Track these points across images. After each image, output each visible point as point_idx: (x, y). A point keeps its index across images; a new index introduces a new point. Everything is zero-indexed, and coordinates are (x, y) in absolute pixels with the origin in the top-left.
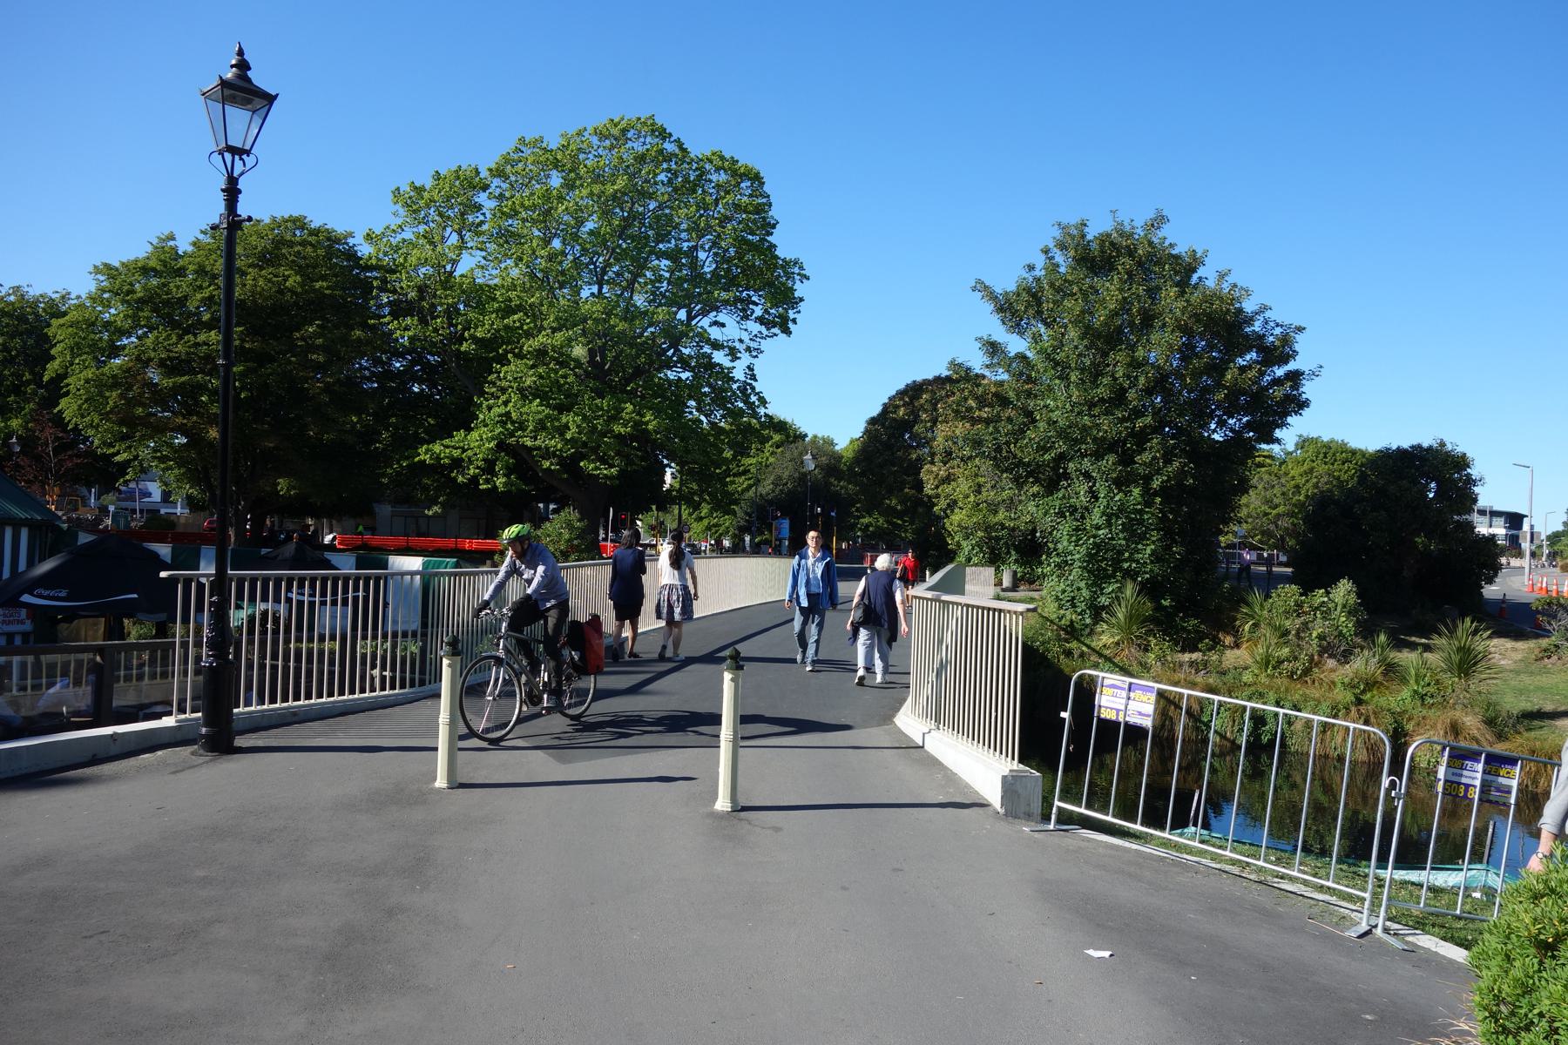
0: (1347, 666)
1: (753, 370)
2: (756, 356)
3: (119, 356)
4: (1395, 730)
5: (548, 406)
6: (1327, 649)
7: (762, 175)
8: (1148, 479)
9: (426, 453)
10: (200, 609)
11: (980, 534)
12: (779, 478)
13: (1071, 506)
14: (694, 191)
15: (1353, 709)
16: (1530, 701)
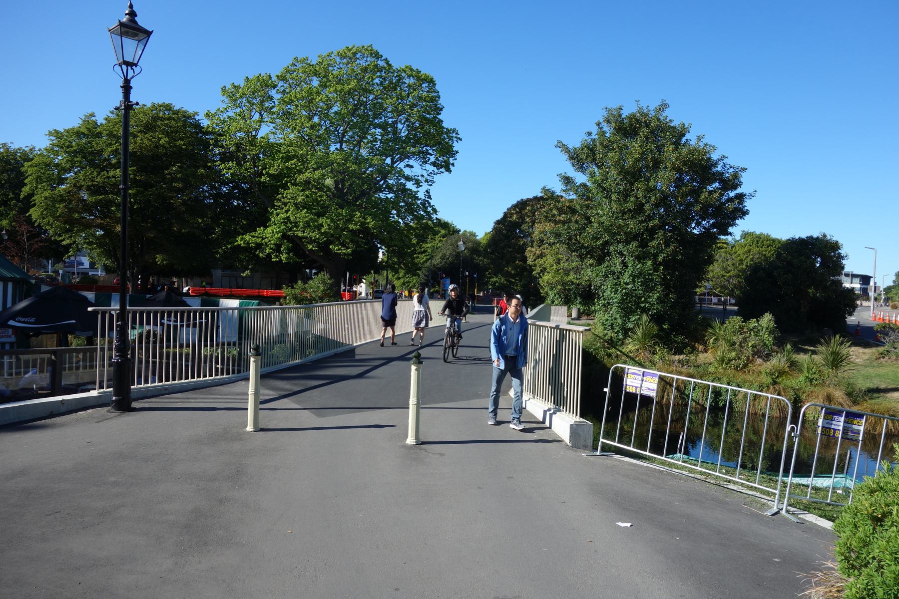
0: (769, 363)
1: (429, 193)
2: (431, 185)
3: (64, 184)
4: (795, 399)
5: (311, 213)
6: (757, 353)
7: (434, 80)
8: (656, 256)
9: (241, 240)
10: (111, 329)
11: (559, 287)
12: (445, 255)
13: (611, 271)
14: (396, 89)
15: (771, 387)
16: (873, 383)
